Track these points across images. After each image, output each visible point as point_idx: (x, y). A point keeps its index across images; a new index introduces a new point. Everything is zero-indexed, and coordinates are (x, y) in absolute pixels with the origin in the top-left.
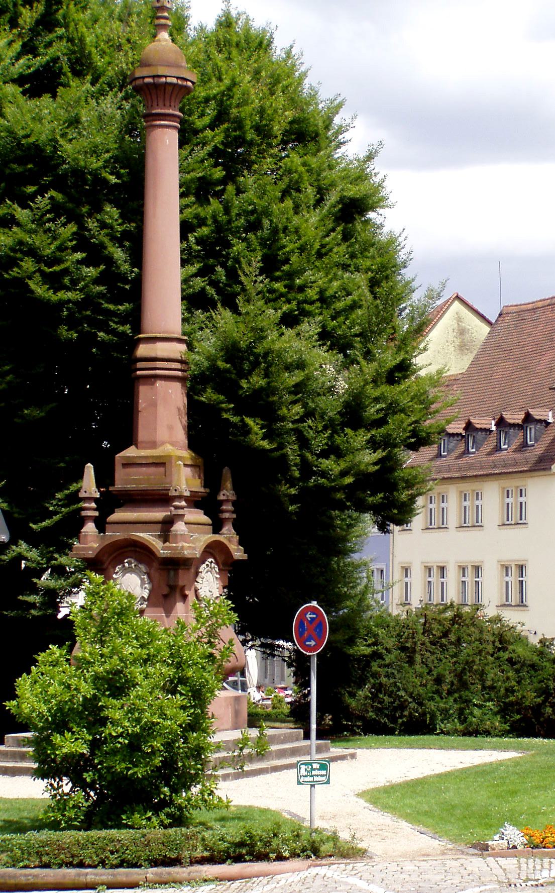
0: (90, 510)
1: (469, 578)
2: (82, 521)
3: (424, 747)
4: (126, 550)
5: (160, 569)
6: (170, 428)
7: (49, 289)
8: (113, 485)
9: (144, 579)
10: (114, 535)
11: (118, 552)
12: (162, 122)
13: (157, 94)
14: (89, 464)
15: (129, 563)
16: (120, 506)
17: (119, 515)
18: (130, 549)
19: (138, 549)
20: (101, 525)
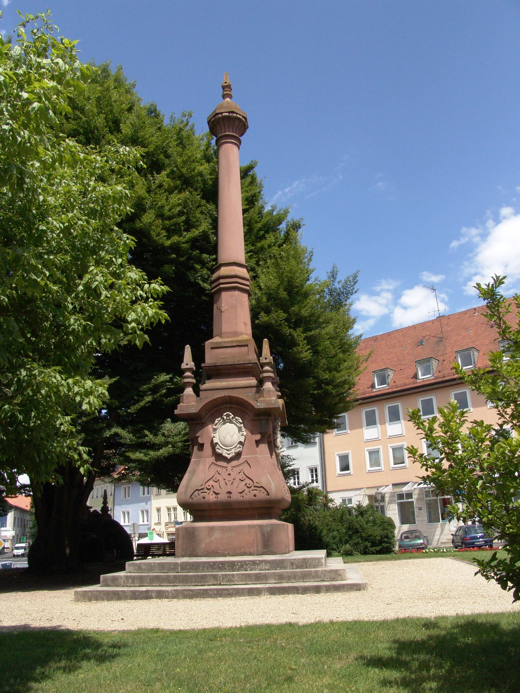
0: (189, 378)
1: (172, 512)
2: (181, 389)
3: (356, 562)
4: (222, 407)
5: (253, 420)
6: (245, 324)
7: (74, 672)
8: (204, 362)
9: (241, 427)
10: (207, 397)
11: (215, 409)
12: (230, 140)
13: (224, 122)
14: (188, 346)
15: (228, 416)
16: (209, 378)
17: (209, 384)
18: (225, 406)
19: (234, 406)
20: (197, 391)
